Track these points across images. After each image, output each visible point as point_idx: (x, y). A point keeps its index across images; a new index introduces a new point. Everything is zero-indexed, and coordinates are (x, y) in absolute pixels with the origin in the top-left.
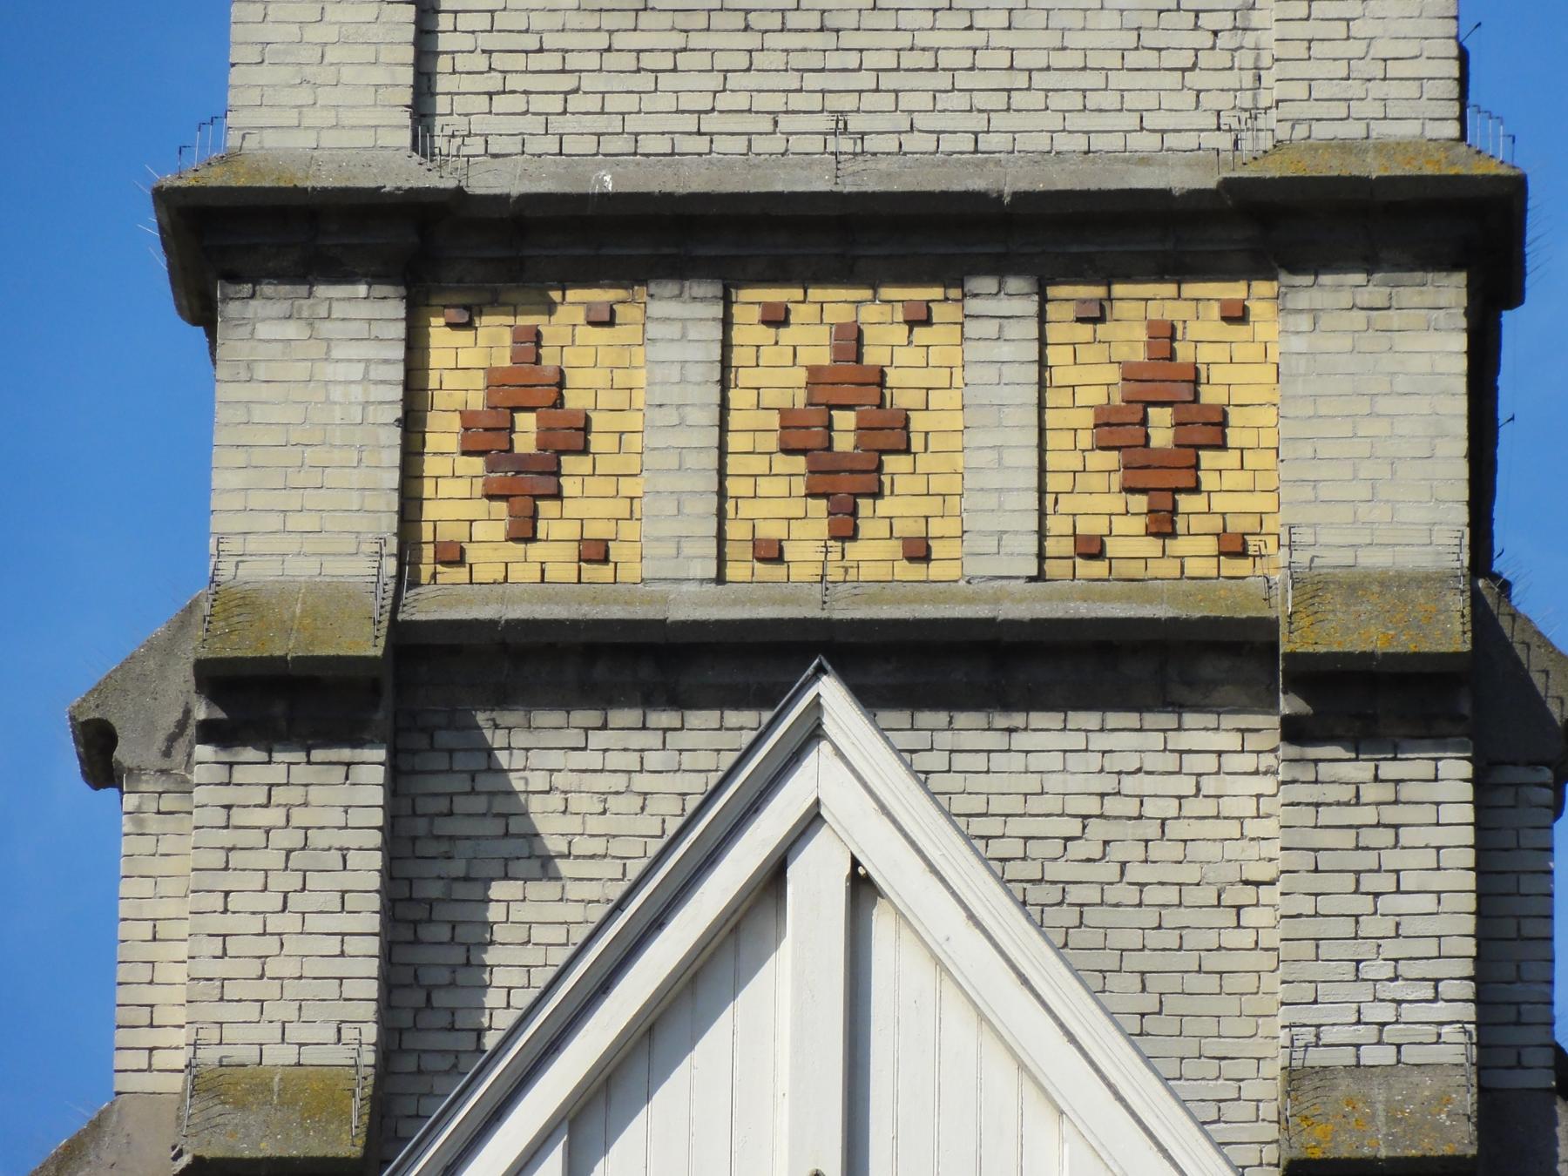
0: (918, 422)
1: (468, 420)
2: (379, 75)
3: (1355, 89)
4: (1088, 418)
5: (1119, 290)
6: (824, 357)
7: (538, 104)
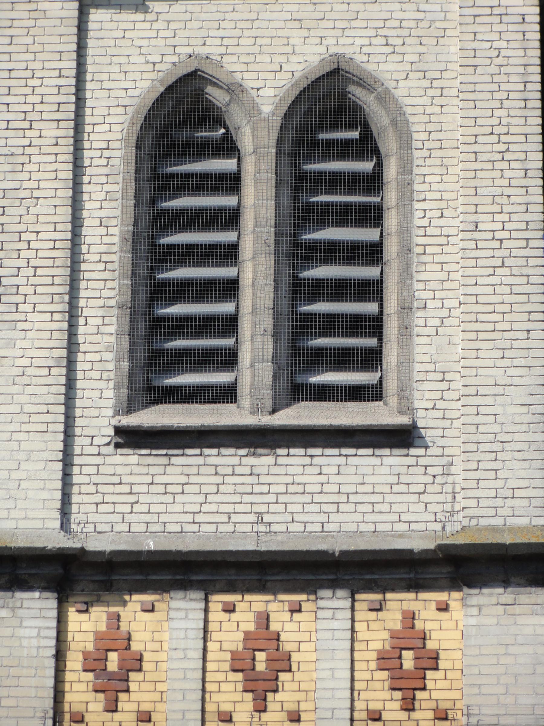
0: (295, 657)
1: (86, 655)
2: (45, 495)
3: (499, 502)
4: (374, 656)
5: (389, 596)
6: (251, 627)
7: (119, 508)
